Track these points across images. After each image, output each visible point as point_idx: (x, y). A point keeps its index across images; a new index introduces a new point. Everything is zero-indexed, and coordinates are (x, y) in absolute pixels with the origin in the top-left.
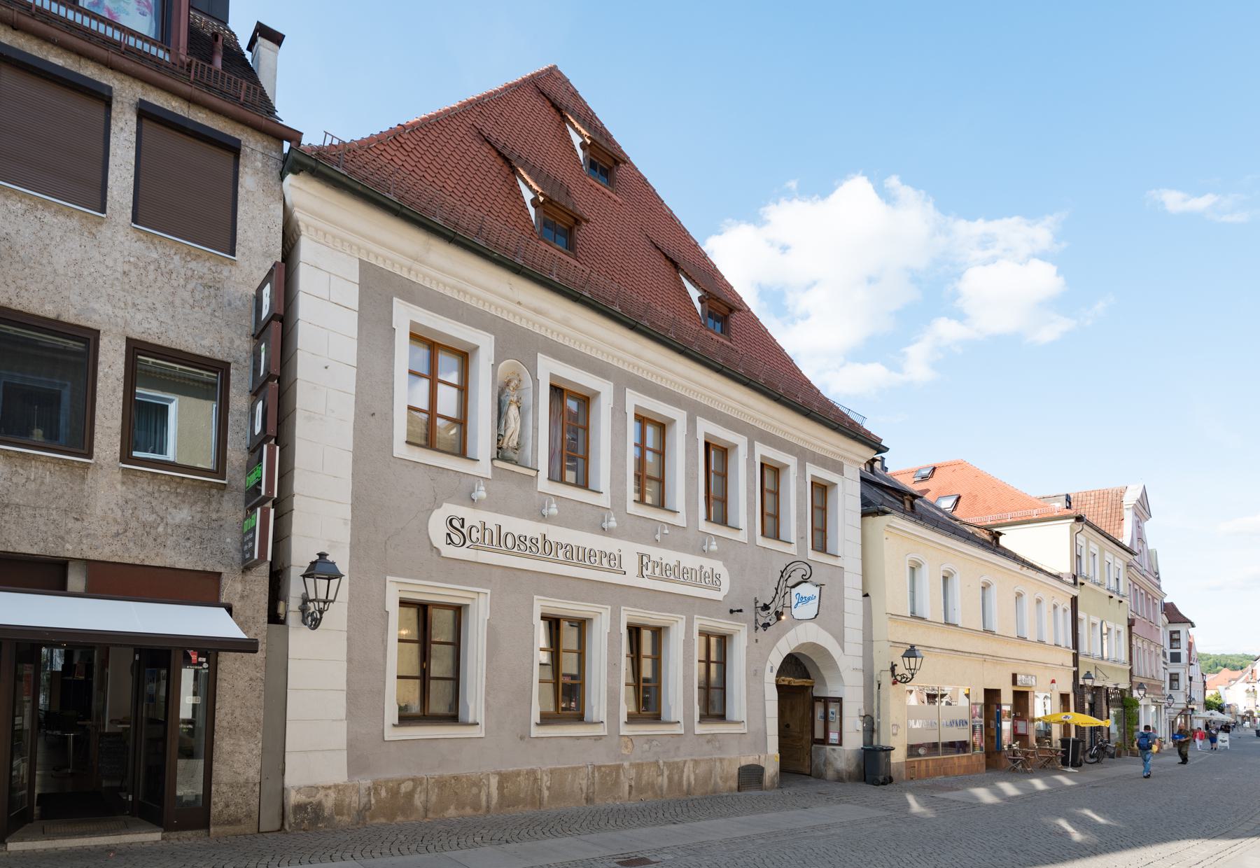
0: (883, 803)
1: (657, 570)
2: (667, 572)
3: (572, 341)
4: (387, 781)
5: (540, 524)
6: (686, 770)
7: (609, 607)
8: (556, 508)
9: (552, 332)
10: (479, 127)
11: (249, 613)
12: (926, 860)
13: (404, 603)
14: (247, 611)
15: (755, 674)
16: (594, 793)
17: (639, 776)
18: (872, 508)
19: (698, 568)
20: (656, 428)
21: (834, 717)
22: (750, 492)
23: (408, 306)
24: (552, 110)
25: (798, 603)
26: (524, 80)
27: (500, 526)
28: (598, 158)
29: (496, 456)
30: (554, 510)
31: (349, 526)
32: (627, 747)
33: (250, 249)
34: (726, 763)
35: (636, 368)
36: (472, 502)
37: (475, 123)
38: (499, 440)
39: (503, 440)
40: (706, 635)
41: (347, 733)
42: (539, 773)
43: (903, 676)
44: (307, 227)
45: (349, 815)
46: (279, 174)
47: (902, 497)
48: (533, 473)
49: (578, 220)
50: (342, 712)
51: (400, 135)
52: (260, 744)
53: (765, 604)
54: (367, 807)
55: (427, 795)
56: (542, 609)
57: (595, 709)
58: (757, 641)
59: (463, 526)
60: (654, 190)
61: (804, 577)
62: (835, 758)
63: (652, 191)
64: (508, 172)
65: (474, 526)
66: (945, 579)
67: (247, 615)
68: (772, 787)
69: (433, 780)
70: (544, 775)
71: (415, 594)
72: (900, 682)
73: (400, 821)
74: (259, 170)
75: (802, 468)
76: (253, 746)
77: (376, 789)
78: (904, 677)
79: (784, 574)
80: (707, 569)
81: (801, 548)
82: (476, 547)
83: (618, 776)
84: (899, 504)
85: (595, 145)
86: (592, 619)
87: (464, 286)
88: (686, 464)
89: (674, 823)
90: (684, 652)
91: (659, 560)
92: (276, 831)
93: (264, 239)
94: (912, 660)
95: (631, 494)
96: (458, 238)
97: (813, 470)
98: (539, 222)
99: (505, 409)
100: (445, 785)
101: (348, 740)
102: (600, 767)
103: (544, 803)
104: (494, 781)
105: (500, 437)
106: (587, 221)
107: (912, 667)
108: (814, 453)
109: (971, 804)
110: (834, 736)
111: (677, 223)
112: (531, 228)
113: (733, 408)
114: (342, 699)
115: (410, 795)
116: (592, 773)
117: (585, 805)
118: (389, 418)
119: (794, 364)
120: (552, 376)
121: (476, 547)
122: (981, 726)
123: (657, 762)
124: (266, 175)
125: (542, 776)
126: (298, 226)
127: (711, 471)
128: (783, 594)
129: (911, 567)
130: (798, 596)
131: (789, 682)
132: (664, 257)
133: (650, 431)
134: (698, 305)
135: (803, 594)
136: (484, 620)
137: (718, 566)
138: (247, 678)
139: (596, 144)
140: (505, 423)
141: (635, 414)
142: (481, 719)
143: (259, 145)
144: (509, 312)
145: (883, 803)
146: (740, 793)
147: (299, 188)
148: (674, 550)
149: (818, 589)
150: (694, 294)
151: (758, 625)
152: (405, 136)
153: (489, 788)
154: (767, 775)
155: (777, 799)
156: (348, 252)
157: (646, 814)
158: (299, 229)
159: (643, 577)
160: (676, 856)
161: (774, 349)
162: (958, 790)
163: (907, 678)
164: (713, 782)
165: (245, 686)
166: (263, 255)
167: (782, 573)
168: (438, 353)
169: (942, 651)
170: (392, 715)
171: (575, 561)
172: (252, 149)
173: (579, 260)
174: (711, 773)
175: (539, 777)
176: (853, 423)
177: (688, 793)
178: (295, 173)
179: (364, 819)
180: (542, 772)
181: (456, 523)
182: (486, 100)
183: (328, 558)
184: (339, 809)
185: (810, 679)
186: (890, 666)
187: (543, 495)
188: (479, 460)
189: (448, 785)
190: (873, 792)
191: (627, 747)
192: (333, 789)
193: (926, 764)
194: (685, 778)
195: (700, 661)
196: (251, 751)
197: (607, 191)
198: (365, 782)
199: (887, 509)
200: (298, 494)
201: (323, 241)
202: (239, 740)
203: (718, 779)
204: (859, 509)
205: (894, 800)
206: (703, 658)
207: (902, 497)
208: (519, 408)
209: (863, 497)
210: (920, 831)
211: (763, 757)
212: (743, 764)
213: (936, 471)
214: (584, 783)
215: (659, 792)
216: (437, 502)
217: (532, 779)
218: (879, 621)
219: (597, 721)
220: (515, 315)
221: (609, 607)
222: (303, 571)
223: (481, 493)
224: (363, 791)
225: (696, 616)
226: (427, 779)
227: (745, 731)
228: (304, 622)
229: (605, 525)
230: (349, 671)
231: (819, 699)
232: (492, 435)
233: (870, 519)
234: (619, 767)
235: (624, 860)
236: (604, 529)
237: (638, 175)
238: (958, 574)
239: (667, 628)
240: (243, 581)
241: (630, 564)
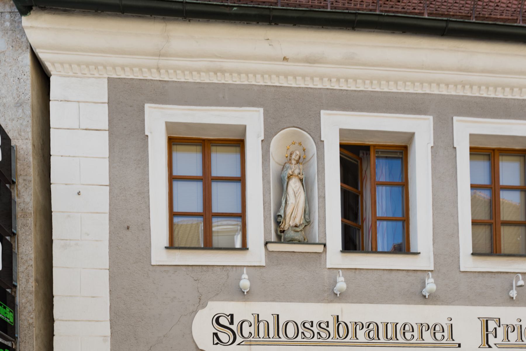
3: (367, 82)
5: (331, 305)
8: (249, 279)
9: (338, 80)
27: (278, 316)
29: (273, 238)
30: (341, 285)
35: (467, 87)
44: (53, 64)
48: (320, 249)
59: (232, 323)
80: (267, 315)
82: (249, 343)
91: (515, 323)
121: (249, 343)
144: (304, 77)
147: (31, 27)
156: (97, 75)
159: (490, 347)
166: (15, 106)
171: (382, 340)
181: (224, 321)
188: (419, 253)
201: (71, 74)
216: (201, 303)
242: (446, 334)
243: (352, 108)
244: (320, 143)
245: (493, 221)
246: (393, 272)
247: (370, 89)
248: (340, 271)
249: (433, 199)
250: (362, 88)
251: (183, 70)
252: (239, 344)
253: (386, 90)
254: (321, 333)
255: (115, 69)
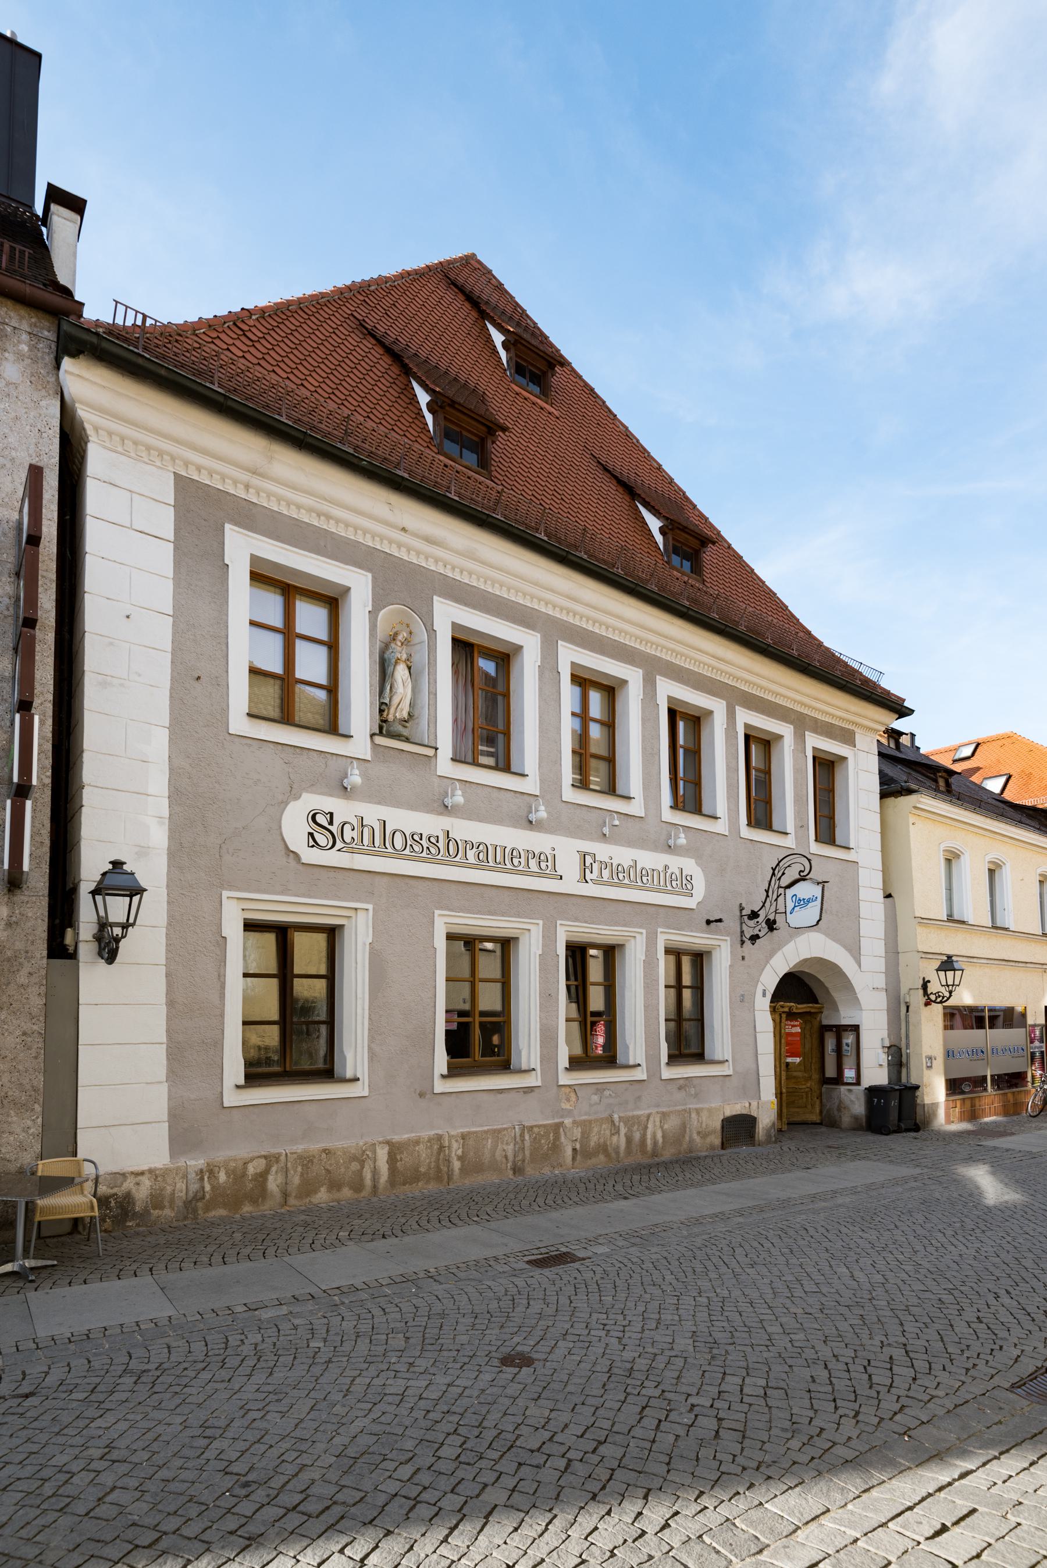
0: (913, 1157)
1: (606, 873)
2: (618, 875)
3: (482, 580)
4: (226, 1163)
5: (441, 817)
6: (650, 1126)
7: (541, 922)
8: (546, 811)
10: (360, 318)
11: (19, 945)
12: (965, 1241)
13: (250, 926)
14: (17, 943)
15: (742, 1000)
16: (524, 1161)
17: (585, 1136)
18: (894, 787)
19: (661, 869)
20: (604, 692)
21: (848, 1050)
22: (731, 770)
23: (248, 536)
24: (467, 305)
25: (795, 906)
26: (429, 267)
27: (384, 822)
28: (525, 361)
30: (459, 798)
31: (166, 827)
32: (568, 1100)
33: (13, 460)
34: (704, 1115)
35: (571, 614)
36: (344, 791)
37: (355, 314)
38: (381, 711)
39: (389, 709)
40: (675, 953)
41: (169, 1099)
42: (447, 1139)
43: (938, 994)
44: (96, 429)
45: (171, 1207)
46: (54, 361)
47: (935, 774)
48: (430, 752)
49: (492, 428)
50: (162, 1072)
51: (243, 321)
52: (40, 1120)
53: (752, 911)
54: (199, 1196)
55: (287, 1177)
56: (447, 927)
57: (524, 1054)
58: (743, 958)
59: (331, 823)
60: (604, 402)
61: (802, 874)
62: (852, 1101)
63: (601, 403)
64: (390, 363)
65: (349, 823)
66: (991, 872)
67: (16, 948)
68: (768, 1141)
69: (295, 1156)
70: (453, 1141)
71: (264, 913)
72: (935, 1002)
73: (247, 1212)
74: (24, 355)
75: (800, 738)
76: (29, 1123)
77: (211, 1172)
78: (939, 996)
79: (776, 872)
80: (674, 869)
81: (802, 839)
83: (557, 1137)
84: (929, 783)
85: (521, 343)
86: (517, 938)
87: (325, 507)
88: (643, 736)
89: (626, 1198)
90: (645, 976)
92: (65, 1235)
93: (32, 446)
94: (950, 974)
95: (568, 774)
96: (310, 440)
97: (815, 741)
98: (438, 433)
99: (390, 670)
100: (312, 1161)
101: (169, 1108)
102: (531, 1128)
103: (455, 1178)
104: (382, 1154)
105: (384, 707)
106: (504, 429)
107: (950, 982)
108: (816, 720)
109: (1030, 1152)
110: (849, 1074)
111: (634, 441)
112: (428, 440)
113: (705, 664)
114: (161, 1054)
115: (263, 1176)
116: (521, 1136)
117: (511, 1177)
118: (221, 683)
119: (789, 611)
120: (455, 626)
122: (1042, 1052)
123: (611, 1116)
124: (35, 361)
125: (450, 1141)
126: (84, 429)
127: (678, 746)
128: (775, 896)
129: (946, 859)
130: (794, 898)
131: (790, 1008)
132: (614, 482)
133: (595, 698)
134: (659, 538)
135: (800, 896)
136: (365, 944)
137: (690, 866)
138: (18, 1033)
139: (523, 341)
140: (391, 687)
141: (572, 675)
142: (363, 1073)
143: (24, 322)
145: (913, 1157)
146: (723, 1152)
148: (629, 846)
149: (820, 887)
150: (654, 524)
151: (744, 939)
152: (251, 323)
153: (375, 1161)
154: (761, 1126)
155: (771, 1157)
157: (591, 1186)
158: (86, 434)
159: (587, 882)
160: (614, 1247)
161: (763, 593)
162: (1013, 1134)
163: (943, 997)
164: (687, 1138)
165: (17, 1044)
167: (774, 870)
168: (295, 599)
169: (989, 961)
170: (234, 1069)
171: (491, 864)
172: (15, 328)
173: (496, 480)
174: (685, 1127)
175: (446, 1144)
176: (866, 681)
177: (655, 1154)
178: (73, 355)
179: (195, 1211)
180: (450, 1137)
181: (321, 819)
182: (372, 288)
183: (125, 867)
184: (157, 1200)
185: (817, 1002)
186: (921, 982)
187: (445, 780)
189: (315, 1161)
190: (899, 1143)
191: (568, 1100)
192: (147, 1175)
193: (972, 1103)
194: (649, 1136)
195: (666, 987)
196: (26, 1130)
197: (539, 401)
198: (196, 1162)
199: (914, 786)
200: (89, 785)
201: (120, 449)
202: (8, 1116)
203: (695, 1136)
204: (876, 787)
205: (927, 1152)
206: (672, 982)
207: (935, 774)
208: (409, 668)
209: (881, 773)
210: (960, 1195)
211: (754, 1104)
212: (729, 1112)
213: (980, 747)
214: (510, 1149)
215: (613, 1155)
217: (436, 1147)
218: (904, 924)
219: (527, 1068)
220: (400, 546)
221: (541, 922)
222: (92, 886)
223: (355, 778)
224: (192, 1176)
225: (660, 930)
226: (286, 1154)
227: (730, 1072)
228: (100, 955)
229: (533, 817)
230: (169, 1019)
231: (829, 1028)
232: (371, 704)
233: (891, 801)
234: (558, 1126)
235: (541, 1256)
236: (531, 822)
237: (582, 384)
238: (1008, 865)
239: (622, 946)
240: (10, 904)
241: (569, 866)
242: (549, 864)
243: (603, 652)
244: (432, 632)
245: (583, 752)
246: (502, 791)
247: (482, 587)
248: (355, 762)
249: (540, 721)
250: (475, 584)
251: (279, 499)
252: (339, 850)
253: (498, 593)
254: (431, 848)
255: (187, 467)
